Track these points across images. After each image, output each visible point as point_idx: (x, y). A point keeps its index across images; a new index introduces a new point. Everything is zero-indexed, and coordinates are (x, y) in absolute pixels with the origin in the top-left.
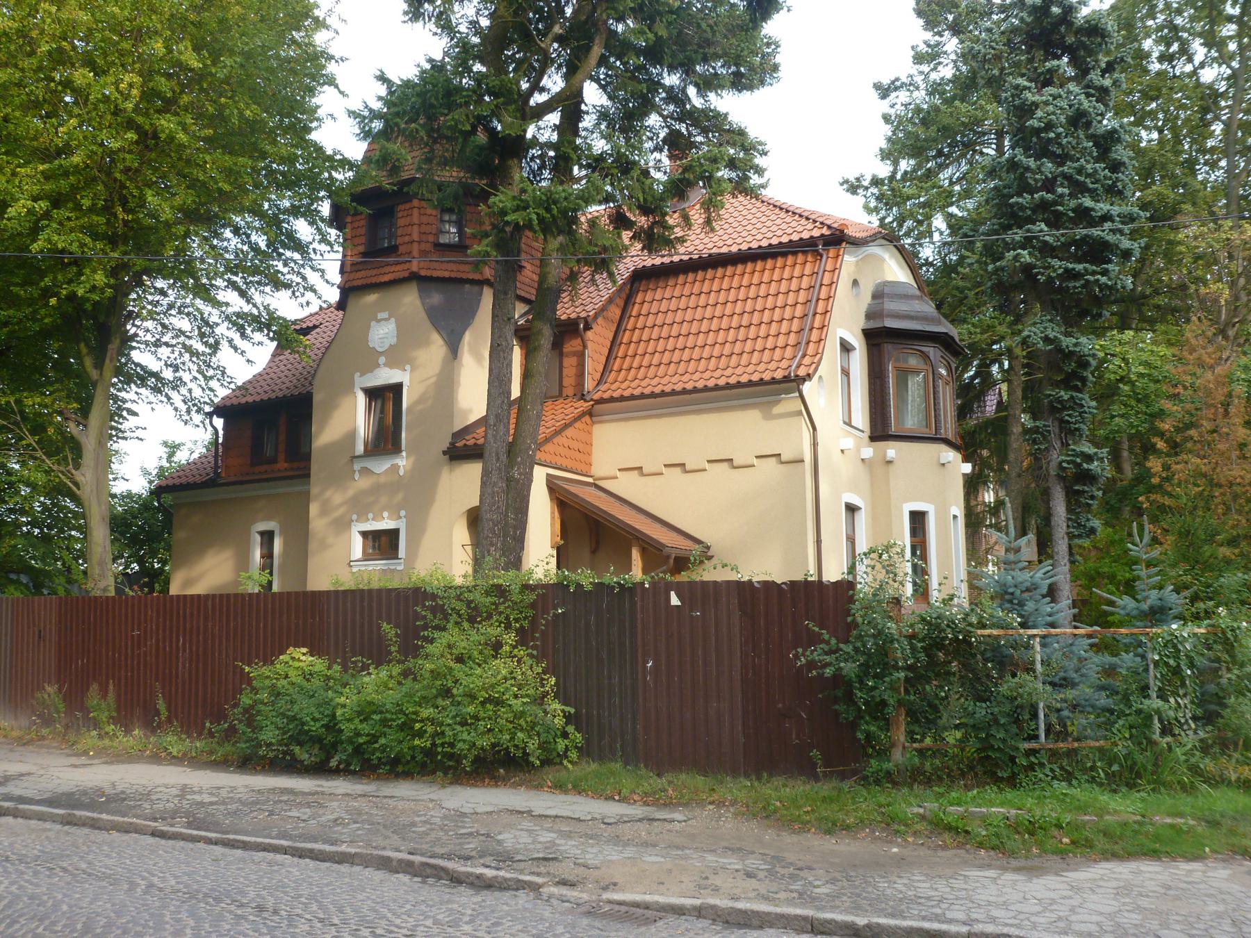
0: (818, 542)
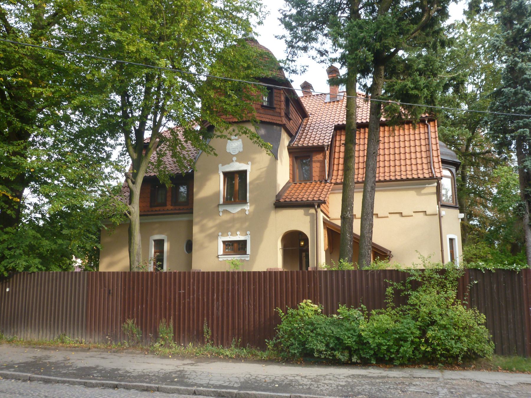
0: (442, 251)
